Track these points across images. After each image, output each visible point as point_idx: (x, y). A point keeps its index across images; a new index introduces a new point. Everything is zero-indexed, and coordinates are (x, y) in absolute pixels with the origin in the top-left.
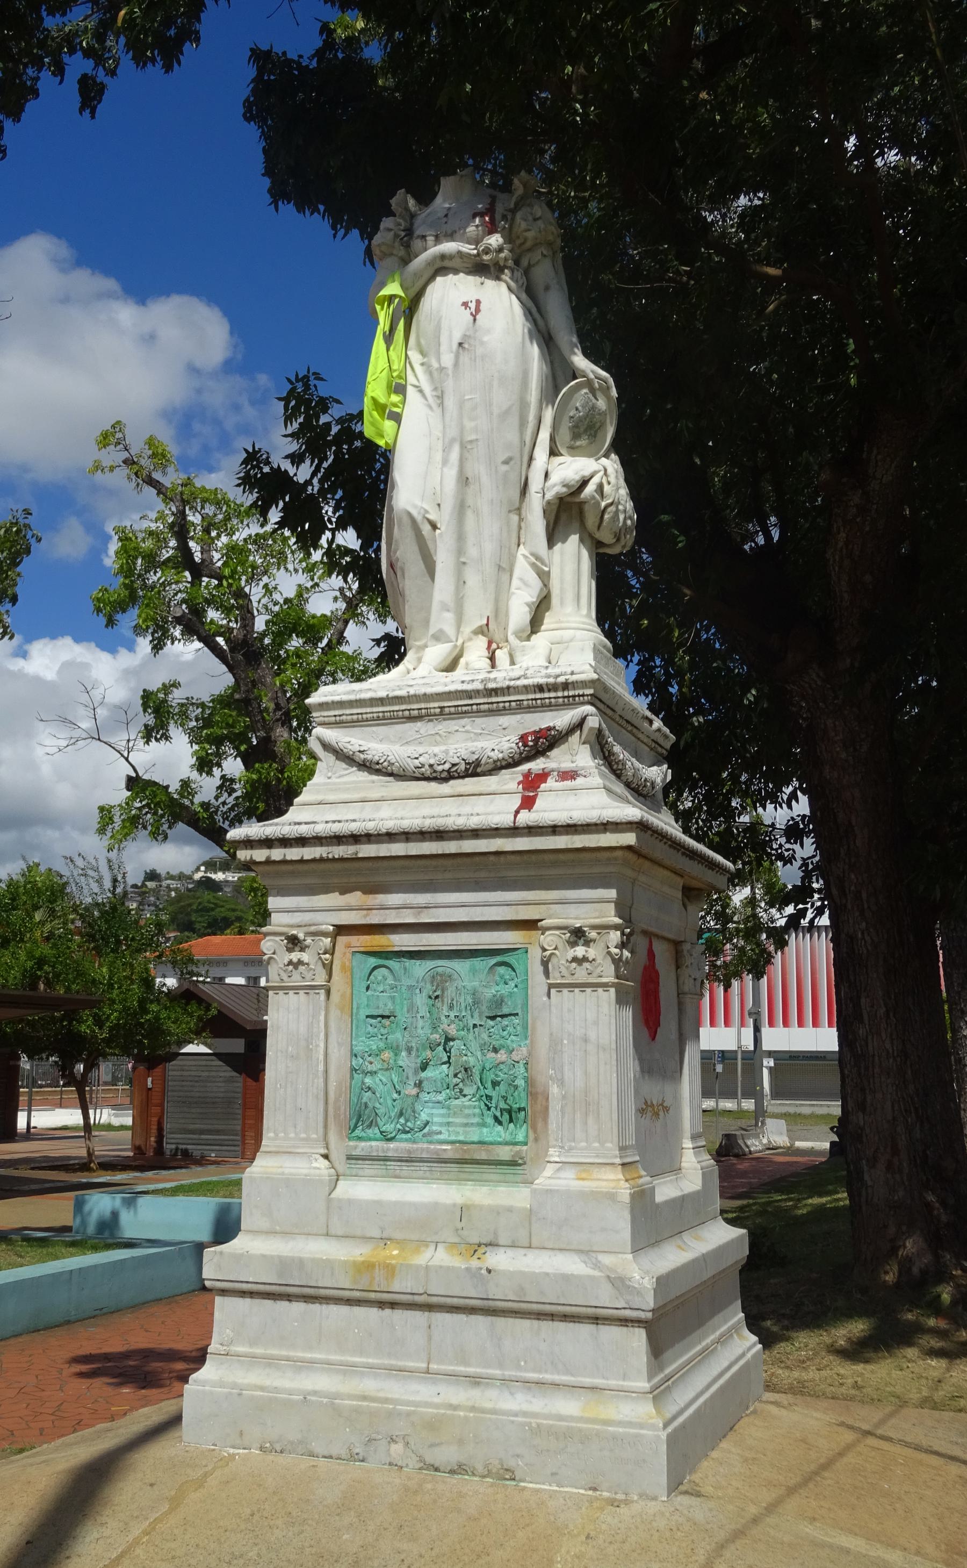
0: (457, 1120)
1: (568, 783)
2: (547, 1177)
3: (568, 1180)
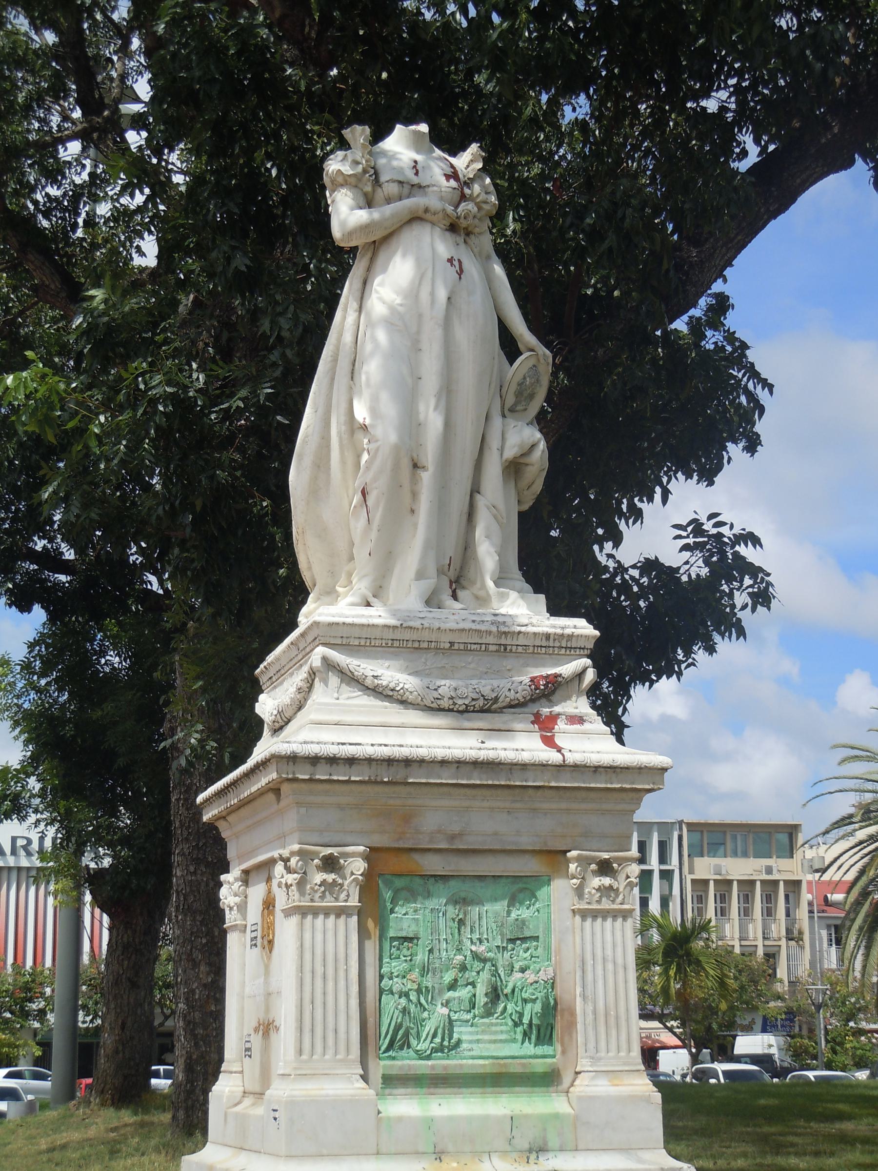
0: (486, 1037)
1: (577, 727)
2: (584, 1086)
3: (602, 1087)
